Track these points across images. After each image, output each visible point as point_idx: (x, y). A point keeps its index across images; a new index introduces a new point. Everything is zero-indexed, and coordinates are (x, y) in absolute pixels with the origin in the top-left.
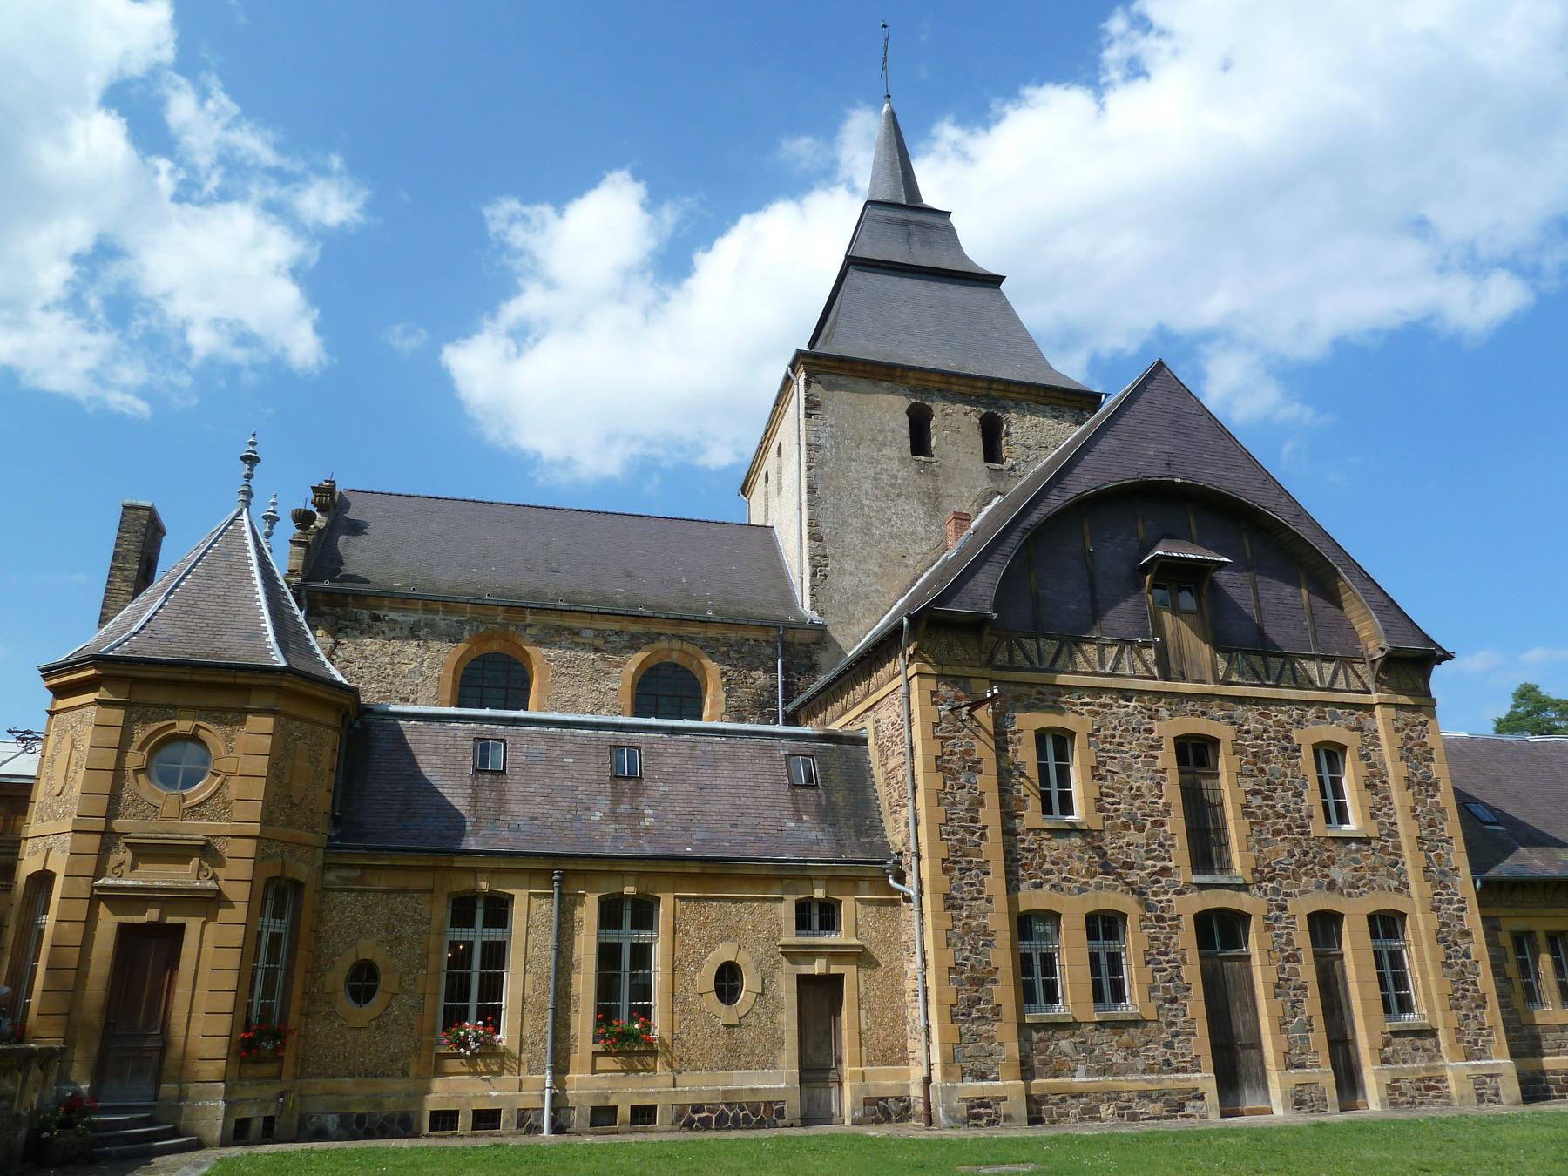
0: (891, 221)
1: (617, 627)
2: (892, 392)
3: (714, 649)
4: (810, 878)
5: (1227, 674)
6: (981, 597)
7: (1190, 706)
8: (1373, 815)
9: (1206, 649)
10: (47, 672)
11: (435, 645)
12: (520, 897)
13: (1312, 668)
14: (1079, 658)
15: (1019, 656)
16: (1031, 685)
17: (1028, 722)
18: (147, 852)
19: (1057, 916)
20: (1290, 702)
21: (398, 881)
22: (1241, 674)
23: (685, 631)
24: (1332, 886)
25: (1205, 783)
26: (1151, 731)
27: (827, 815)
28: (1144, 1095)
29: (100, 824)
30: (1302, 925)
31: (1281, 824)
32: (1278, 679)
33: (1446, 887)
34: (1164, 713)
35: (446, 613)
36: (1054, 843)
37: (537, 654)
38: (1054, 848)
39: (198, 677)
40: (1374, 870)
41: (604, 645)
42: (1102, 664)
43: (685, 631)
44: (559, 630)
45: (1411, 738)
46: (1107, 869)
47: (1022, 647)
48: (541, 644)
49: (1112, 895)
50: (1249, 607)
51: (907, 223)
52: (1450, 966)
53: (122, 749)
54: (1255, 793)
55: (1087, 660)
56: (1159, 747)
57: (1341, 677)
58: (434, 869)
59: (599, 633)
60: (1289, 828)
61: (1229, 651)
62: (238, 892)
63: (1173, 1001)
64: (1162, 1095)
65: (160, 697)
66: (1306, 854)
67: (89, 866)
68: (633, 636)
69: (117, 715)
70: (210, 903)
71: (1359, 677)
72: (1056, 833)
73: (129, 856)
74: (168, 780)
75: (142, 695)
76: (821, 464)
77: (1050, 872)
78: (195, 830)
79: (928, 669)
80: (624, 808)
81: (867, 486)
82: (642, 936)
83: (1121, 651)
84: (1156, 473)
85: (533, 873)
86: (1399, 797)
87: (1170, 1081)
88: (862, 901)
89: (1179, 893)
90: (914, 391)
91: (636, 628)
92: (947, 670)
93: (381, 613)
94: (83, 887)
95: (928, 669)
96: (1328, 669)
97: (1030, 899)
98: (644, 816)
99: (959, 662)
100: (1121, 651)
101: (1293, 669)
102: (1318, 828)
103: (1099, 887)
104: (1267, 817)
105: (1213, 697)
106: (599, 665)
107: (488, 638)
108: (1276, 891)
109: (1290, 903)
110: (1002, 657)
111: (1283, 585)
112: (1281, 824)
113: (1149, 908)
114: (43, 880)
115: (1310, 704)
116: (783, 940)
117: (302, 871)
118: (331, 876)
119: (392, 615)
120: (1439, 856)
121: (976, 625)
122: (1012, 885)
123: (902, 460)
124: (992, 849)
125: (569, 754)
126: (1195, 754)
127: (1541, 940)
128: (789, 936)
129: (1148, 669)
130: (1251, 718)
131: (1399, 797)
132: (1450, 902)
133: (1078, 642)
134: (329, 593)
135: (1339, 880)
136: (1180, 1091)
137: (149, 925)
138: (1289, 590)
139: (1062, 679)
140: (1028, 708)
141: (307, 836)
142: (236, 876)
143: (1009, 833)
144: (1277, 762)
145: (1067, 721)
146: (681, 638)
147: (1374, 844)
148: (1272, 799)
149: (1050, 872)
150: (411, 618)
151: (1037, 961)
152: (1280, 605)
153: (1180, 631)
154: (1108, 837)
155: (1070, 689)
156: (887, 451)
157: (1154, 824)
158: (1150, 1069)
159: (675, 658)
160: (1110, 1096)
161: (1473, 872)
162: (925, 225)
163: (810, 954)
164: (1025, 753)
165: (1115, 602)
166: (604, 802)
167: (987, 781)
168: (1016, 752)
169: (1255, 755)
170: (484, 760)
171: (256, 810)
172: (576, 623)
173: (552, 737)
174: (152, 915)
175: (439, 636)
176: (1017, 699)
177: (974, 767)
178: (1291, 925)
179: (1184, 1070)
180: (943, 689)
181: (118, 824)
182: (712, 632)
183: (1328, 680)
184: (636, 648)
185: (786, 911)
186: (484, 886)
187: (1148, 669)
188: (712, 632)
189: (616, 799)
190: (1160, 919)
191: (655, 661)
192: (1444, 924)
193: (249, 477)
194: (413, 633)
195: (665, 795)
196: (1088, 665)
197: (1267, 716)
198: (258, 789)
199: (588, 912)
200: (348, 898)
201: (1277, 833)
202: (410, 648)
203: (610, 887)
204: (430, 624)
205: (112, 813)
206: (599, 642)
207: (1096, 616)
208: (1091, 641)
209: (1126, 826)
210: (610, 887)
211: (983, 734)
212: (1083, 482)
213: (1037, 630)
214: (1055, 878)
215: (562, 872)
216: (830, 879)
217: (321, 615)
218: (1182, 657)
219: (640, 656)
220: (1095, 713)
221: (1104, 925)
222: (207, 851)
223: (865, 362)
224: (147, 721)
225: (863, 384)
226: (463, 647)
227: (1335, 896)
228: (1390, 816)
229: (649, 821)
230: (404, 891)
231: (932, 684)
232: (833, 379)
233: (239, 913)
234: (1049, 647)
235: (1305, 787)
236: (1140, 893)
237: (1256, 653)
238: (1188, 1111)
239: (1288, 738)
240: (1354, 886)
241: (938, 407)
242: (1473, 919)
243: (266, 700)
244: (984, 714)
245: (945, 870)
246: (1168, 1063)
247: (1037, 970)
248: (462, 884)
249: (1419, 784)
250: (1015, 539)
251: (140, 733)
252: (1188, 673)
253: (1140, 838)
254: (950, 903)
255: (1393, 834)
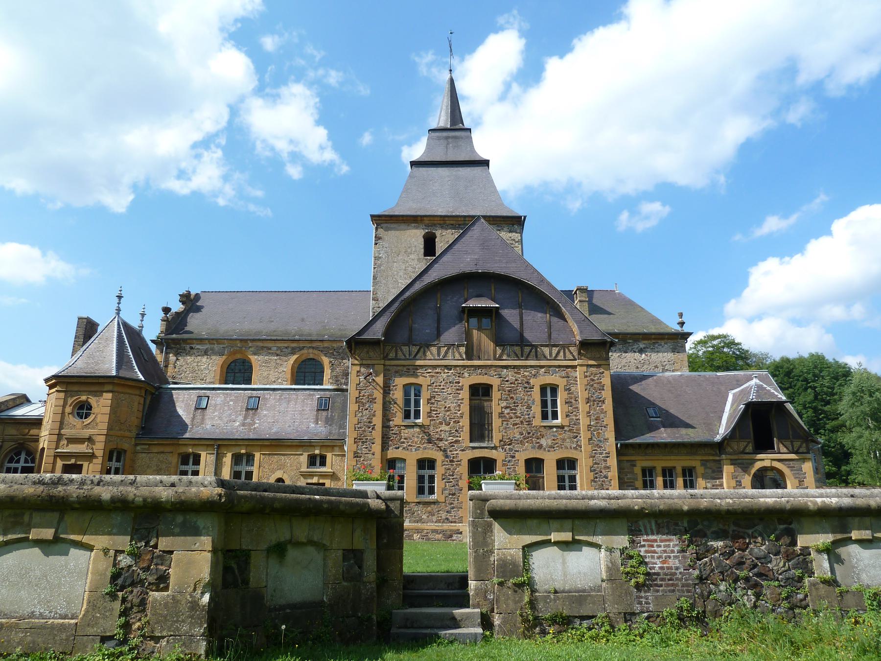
0: (439, 138)
1: (286, 345)
2: (417, 228)
3: (327, 352)
4: (314, 446)
5: (501, 355)
6: (378, 331)
7: (479, 371)
8: (567, 416)
9: (492, 345)
10: (46, 380)
11: (214, 357)
12: (203, 455)
13: (546, 350)
14: (428, 353)
15: (400, 354)
16: (404, 366)
17: (400, 382)
18: (72, 440)
19: (405, 460)
20: (531, 366)
21: (161, 449)
22: (508, 356)
23: (314, 345)
24: (540, 447)
25: (486, 404)
26: (459, 383)
27: (328, 421)
28: (434, 531)
29: (57, 432)
30: (522, 464)
31: (518, 421)
32: (527, 357)
33: (600, 447)
34: (466, 375)
35: (218, 344)
36: (406, 431)
37: (254, 359)
38: (406, 433)
39: (101, 381)
40: (564, 440)
41: (281, 353)
42: (439, 355)
43: (314, 345)
44: (263, 348)
45: (593, 380)
46: (430, 441)
47: (401, 350)
48: (255, 354)
49: (430, 451)
50: (516, 324)
51: (447, 138)
52: (595, 482)
53: (64, 406)
54: (506, 408)
55: (431, 354)
56: (462, 389)
57: (562, 354)
58: (173, 444)
59: (279, 348)
60: (522, 422)
61: (504, 346)
62: (99, 453)
63: (454, 494)
64: (442, 532)
65: (76, 388)
66: (529, 433)
67: (54, 445)
68: (293, 349)
69: (62, 395)
70: (91, 457)
71: (571, 353)
72: (407, 427)
73: (65, 442)
74: (80, 416)
75: (71, 388)
76: (380, 266)
77: (404, 443)
78: (86, 433)
79: (356, 362)
80: (248, 421)
81: (401, 274)
82: (573, 472)
83: (448, 349)
84: (468, 269)
85: (208, 445)
86: (582, 407)
87: (446, 526)
88: (335, 455)
89: (463, 450)
90: (427, 226)
91: (294, 345)
92: (364, 362)
93: (193, 346)
94: (52, 453)
95: (356, 362)
96: (555, 350)
97: (392, 453)
98: (255, 423)
99: (370, 358)
100: (448, 349)
101: (536, 352)
102: (538, 421)
103: (425, 448)
104: (511, 418)
105: (491, 366)
106: (278, 361)
107: (235, 353)
108: (510, 450)
109: (517, 455)
110: (392, 355)
111: (536, 313)
112: (518, 421)
113: (447, 457)
114: (43, 449)
115: (542, 367)
116: (302, 470)
117: (126, 446)
118: (138, 448)
119: (198, 347)
120: (599, 433)
121: (375, 343)
122: (385, 447)
123: (419, 260)
124: (377, 434)
125: (231, 400)
126: (480, 392)
127: (659, 470)
128: (304, 469)
129: (461, 356)
130: (510, 375)
131: (582, 407)
132: (601, 454)
133: (428, 346)
134: (173, 340)
135: (545, 444)
136: (451, 530)
137: (72, 464)
138: (540, 315)
139: (418, 363)
140: (401, 376)
141: (127, 434)
142: (99, 448)
143: (386, 426)
144: (521, 393)
145: (420, 380)
146: (313, 348)
147: (566, 428)
148: (515, 410)
149: (404, 443)
150: (205, 347)
151: (426, 478)
152: (534, 324)
153: (484, 340)
154: (432, 428)
155: (422, 366)
156: (412, 256)
157: (455, 422)
158: (438, 521)
159: (311, 356)
160: (418, 531)
161: (616, 439)
162: (455, 138)
163: (311, 475)
164: (398, 395)
165: (447, 329)
166: (241, 418)
167: (378, 407)
168: (393, 394)
169: (509, 391)
170: (200, 404)
171: (105, 426)
172: (269, 345)
173: (227, 394)
174: (73, 461)
175: (215, 353)
176: (396, 372)
177: (372, 400)
178: (516, 463)
179: (455, 522)
180: (363, 370)
181: (63, 432)
182: (326, 345)
183: (554, 355)
184: (293, 353)
185: (304, 459)
186: (190, 450)
187: (461, 356)
188: (326, 345)
189: (245, 418)
190: (452, 461)
191: (304, 358)
192: (596, 463)
193: (119, 303)
194: (206, 353)
195: (265, 415)
196: (431, 357)
197: (519, 373)
198: (106, 418)
199: (228, 460)
200: (144, 455)
201: (514, 425)
202: (204, 359)
203: (236, 450)
204: (212, 349)
205: (61, 428)
206: (278, 352)
207: (439, 335)
208: (434, 345)
209: (441, 423)
210: (236, 450)
211: (378, 388)
212: (428, 279)
213: (410, 342)
214: (405, 445)
215: (218, 445)
216: (322, 446)
217: (171, 348)
218: (480, 349)
219: (295, 357)
220: (433, 376)
221: (426, 464)
222: (90, 440)
223: (403, 216)
224: (72, 396)
225: (403, 226)
226: (224, 357)
227: (541, 451)
228: (576, 416)
229: (256, 425)
230: (163, 452)
231: (358, 368)
232: (388, 225)
233: (100, 460)
234: (415, 349)
235: (533, 403)
236: (445, 451)
237: (517, 345)
238: (454, 538)
239: (528, 383)
240: (552, 447)
241: (438, 233)
242: (613, 462)
243: (110, 387)
244: (380, 380)
245: (355, 442)
246: (447, 519)
247: (426, 481)
248: (183, 450)
249: (594, 401)
250: (396, 305)
251: (70, 401)
252: (482, 356)
253: (447, 428)
254: (356, 455)
255: (577, 423)
